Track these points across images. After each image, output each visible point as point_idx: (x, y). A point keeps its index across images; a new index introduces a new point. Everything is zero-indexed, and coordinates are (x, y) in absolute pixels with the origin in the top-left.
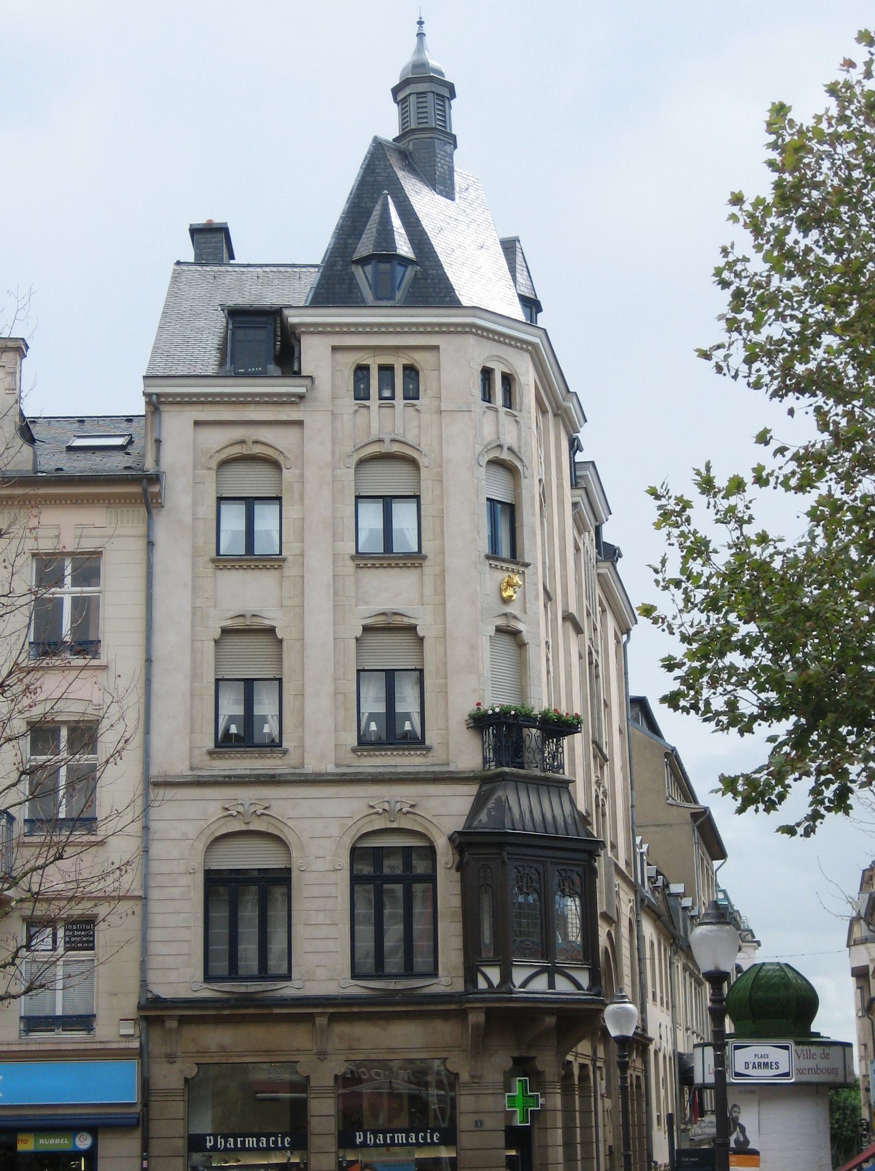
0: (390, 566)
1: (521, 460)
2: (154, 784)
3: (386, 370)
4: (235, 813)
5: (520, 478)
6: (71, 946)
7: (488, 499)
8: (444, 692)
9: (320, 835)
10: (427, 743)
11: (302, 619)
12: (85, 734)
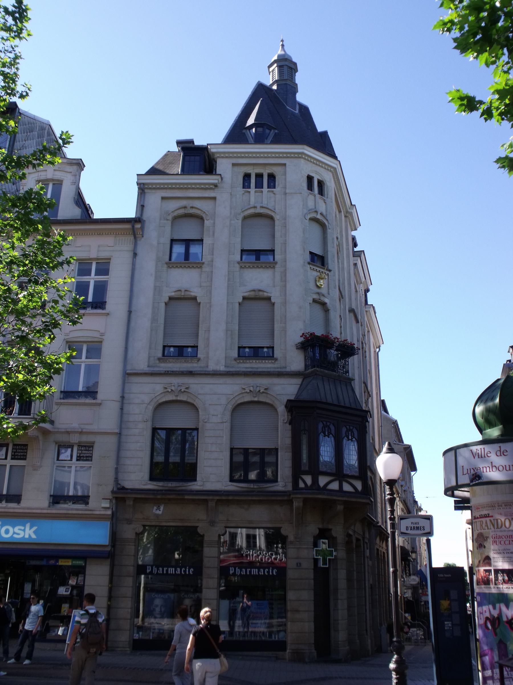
0: (258, 267)
1: (327, 220)
2: (128, 375)
3: (259, 176)
4: (170, 390)
5: (326, 229)
6: (79, 459)
7: (311, 253)
8: (284, 330)
9: (215, 399)
10: (275, 356)
11: (211, 293)
12: (95, 349)
